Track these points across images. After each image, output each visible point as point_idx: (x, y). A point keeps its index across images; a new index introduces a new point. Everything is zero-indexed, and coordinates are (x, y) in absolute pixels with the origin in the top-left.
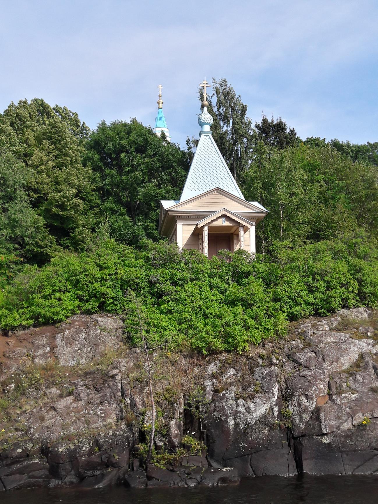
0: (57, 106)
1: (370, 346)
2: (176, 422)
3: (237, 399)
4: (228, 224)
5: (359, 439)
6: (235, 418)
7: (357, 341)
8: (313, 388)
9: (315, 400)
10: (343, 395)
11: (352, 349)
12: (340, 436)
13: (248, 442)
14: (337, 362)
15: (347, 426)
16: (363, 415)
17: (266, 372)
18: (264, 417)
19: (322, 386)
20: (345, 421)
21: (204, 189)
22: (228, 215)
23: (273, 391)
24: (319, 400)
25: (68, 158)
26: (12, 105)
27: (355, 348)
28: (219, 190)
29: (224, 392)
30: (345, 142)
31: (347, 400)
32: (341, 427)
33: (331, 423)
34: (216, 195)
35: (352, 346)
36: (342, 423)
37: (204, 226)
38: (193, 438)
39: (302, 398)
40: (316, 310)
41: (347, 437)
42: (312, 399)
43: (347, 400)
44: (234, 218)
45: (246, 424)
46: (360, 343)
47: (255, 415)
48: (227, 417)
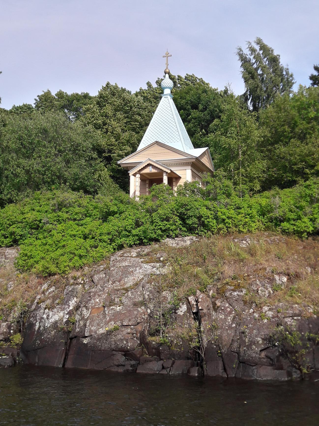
0: (187, 74)
1: (154, 269)
2: (7, 324)
3: (45, 308)
4: (154, 171)
5: (104, 342)
6: (40, 323)
7: (145, 265)
8: (91, 302)
9: (90, 311)
10: (112, 307)
11: (138, 271)
12: (95, 338)
13: (41, 340)
14: (119, 281)
15: (101, 331)
16: (115, 323)
17: (70, 289)
18: (56, 322)
19: (97, 300)
20: (101, 327)
21: (146, 144)
22: (153, 163)
23: (69, 303)
24: (93, 310)
25: (136, 123)
26: (49, 92)
27: (140, 270)
28: (157, 143)
29: (42, 304)
30: (221, 89)
31: (113, 311)
32: (98, 332)
33: (92, 328)
34: (156, 146)
35: (138, 269)
36: (99, 329)
38: (15, 334)
39: (84, 309)
40: (140, 240)
41: (99, 339)
42: (88, 309)
43: (113, 311)
44: (157, 165)
45: (44, 327)
46: (146, 267)
47: (50, 321)
48: (37, 321)
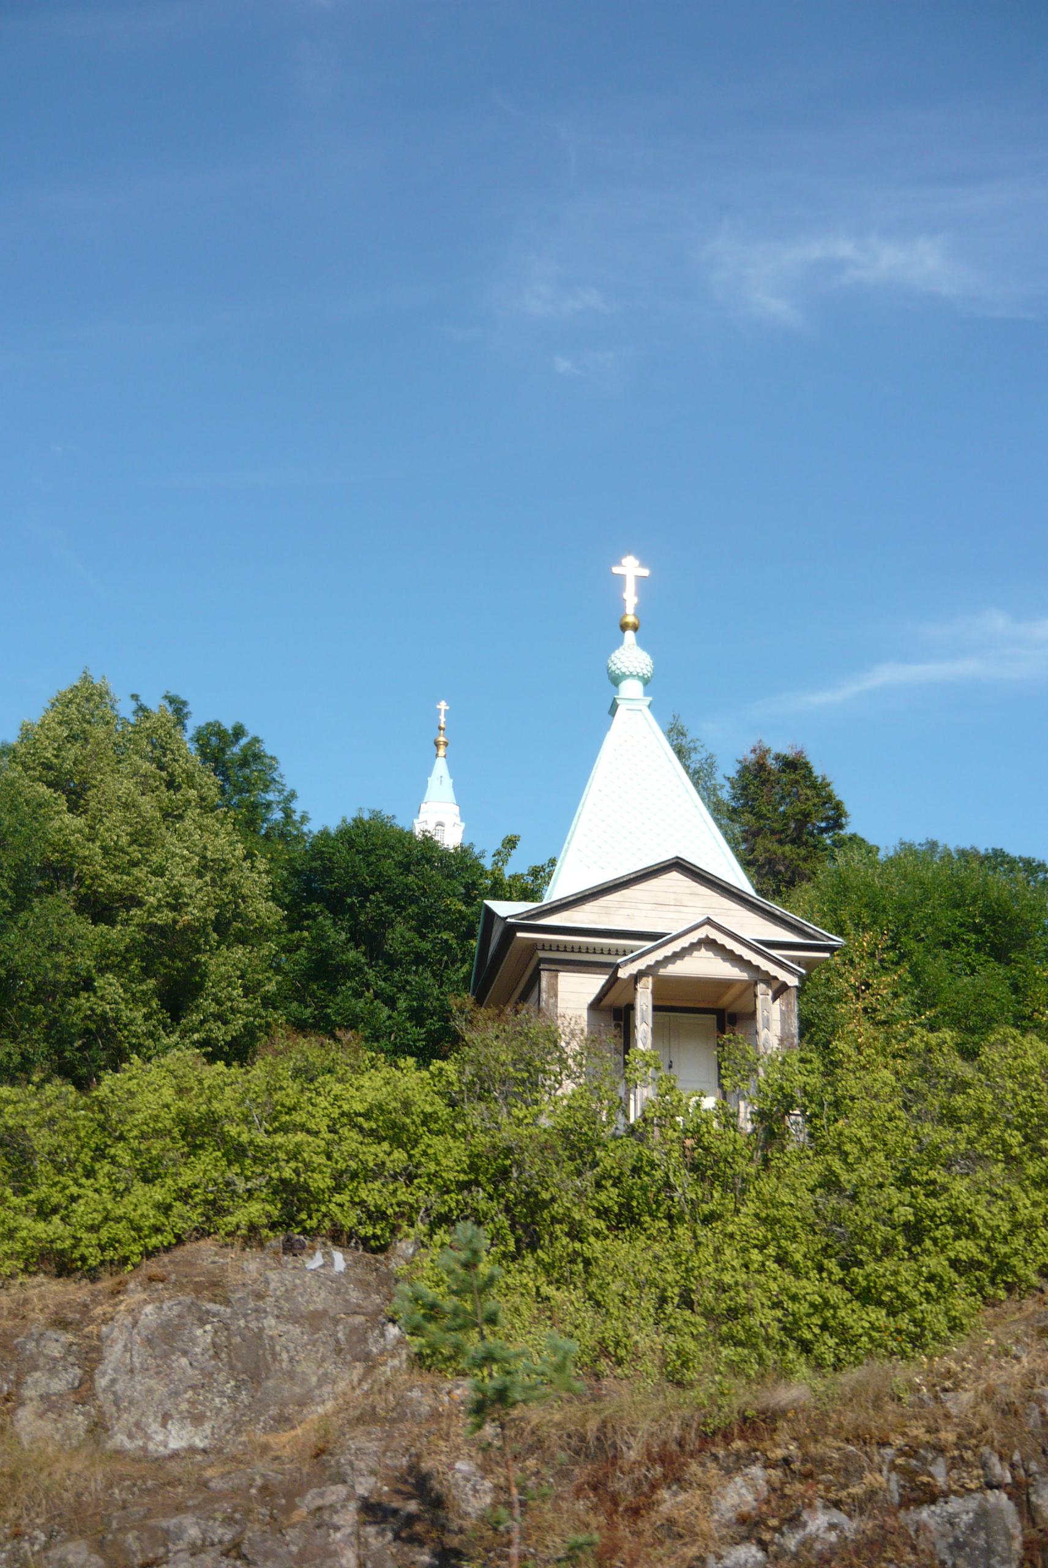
22: (722, 939)
37: (636, 978)
